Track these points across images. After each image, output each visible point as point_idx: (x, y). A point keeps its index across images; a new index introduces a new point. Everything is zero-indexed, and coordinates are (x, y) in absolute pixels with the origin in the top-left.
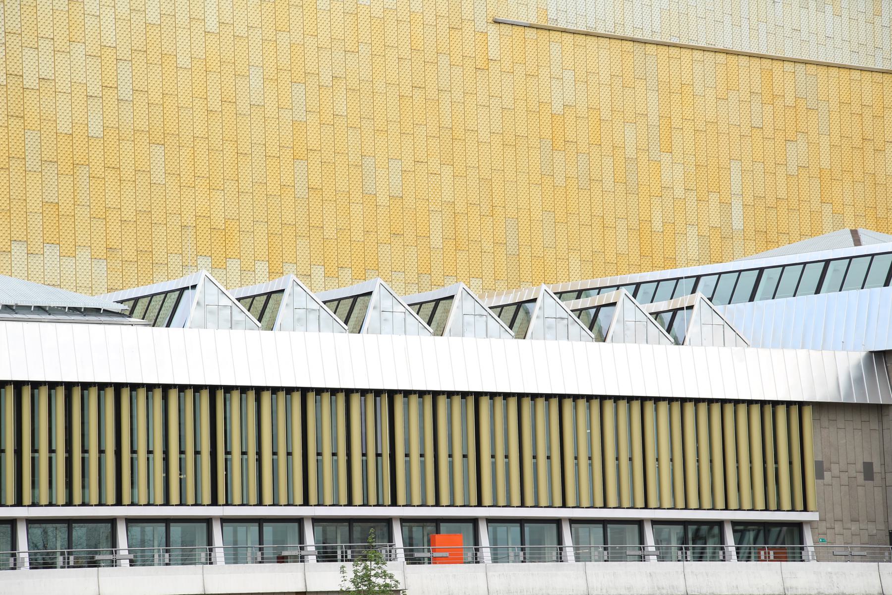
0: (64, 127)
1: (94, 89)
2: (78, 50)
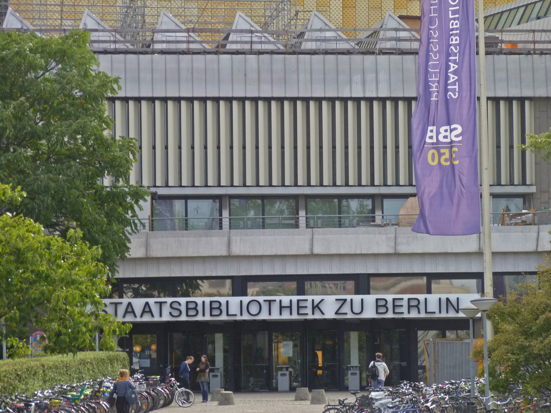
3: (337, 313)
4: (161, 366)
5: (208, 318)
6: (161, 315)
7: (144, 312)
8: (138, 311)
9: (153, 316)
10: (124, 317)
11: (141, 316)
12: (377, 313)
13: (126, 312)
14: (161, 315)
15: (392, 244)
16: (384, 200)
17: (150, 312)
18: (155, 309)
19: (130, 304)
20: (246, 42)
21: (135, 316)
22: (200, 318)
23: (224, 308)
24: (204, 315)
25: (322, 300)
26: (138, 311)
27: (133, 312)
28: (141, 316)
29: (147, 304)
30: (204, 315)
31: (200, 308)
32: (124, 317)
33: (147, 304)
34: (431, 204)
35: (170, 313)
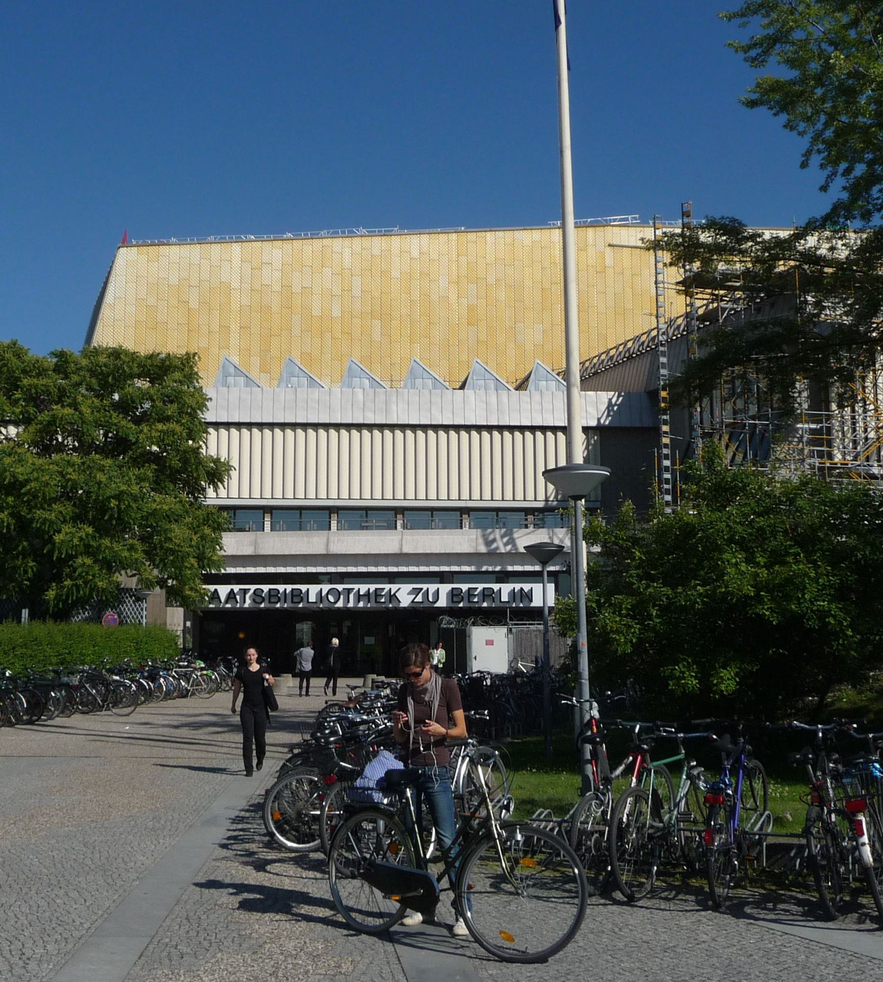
0: (316, 312)
1: (337, 291)
2: (327, 271)
12: (453, 602)
15: (474, 544)
25: (399, 589)
29: (232, 590)
33: (232, 590)
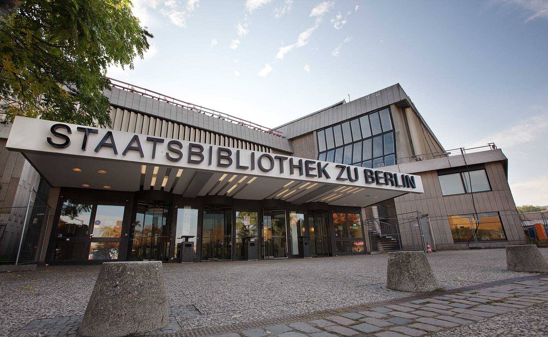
3: (338, 179)
4: (126, 235)
5: (213, 167)
6: (153, 157)
7: (129, 148)
8: (121, 145)
9: (142, 156)
10: (97, 150)
11: (124, 154)
13: (102, 145)
14: (153, 157)
16: (484, 170)
17: (139, 149)
18: (147, 148)
19: (109, 134)
20: (471, 225)
21: (116, 152)
22: (203, 166)
23: (233, 157)
24: (210, 163)
25: (328, 164)
26: (121, 145)
27: (112, 146)
28: (124, 154)
30: (210, 163)
31: (205, 153)
32: (97, 150)
34: (136, 264)
35: (49, 140)
